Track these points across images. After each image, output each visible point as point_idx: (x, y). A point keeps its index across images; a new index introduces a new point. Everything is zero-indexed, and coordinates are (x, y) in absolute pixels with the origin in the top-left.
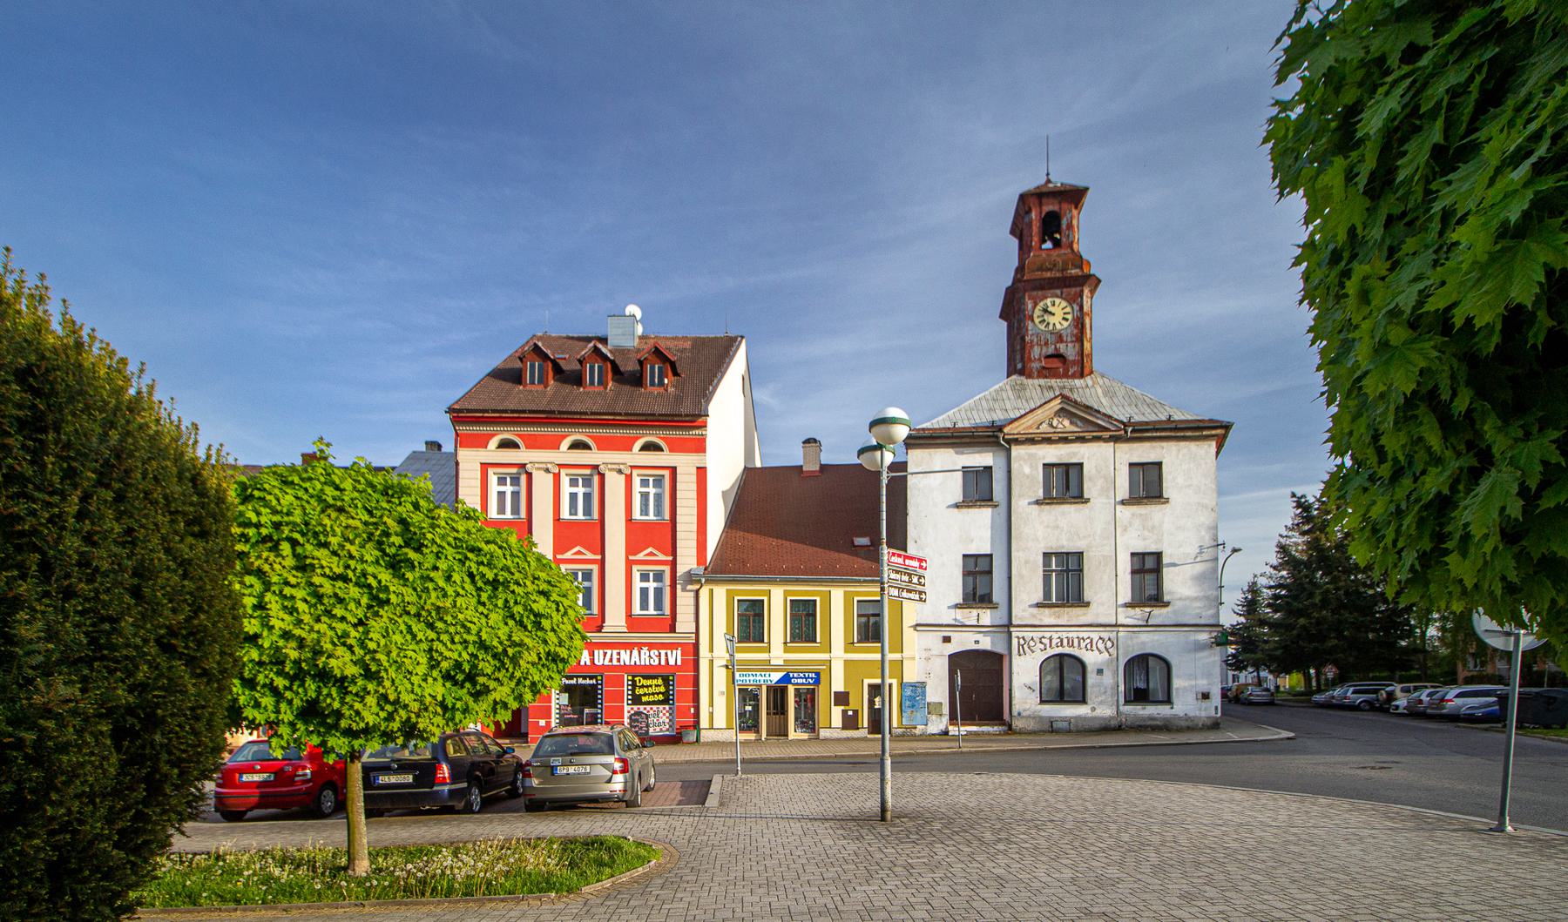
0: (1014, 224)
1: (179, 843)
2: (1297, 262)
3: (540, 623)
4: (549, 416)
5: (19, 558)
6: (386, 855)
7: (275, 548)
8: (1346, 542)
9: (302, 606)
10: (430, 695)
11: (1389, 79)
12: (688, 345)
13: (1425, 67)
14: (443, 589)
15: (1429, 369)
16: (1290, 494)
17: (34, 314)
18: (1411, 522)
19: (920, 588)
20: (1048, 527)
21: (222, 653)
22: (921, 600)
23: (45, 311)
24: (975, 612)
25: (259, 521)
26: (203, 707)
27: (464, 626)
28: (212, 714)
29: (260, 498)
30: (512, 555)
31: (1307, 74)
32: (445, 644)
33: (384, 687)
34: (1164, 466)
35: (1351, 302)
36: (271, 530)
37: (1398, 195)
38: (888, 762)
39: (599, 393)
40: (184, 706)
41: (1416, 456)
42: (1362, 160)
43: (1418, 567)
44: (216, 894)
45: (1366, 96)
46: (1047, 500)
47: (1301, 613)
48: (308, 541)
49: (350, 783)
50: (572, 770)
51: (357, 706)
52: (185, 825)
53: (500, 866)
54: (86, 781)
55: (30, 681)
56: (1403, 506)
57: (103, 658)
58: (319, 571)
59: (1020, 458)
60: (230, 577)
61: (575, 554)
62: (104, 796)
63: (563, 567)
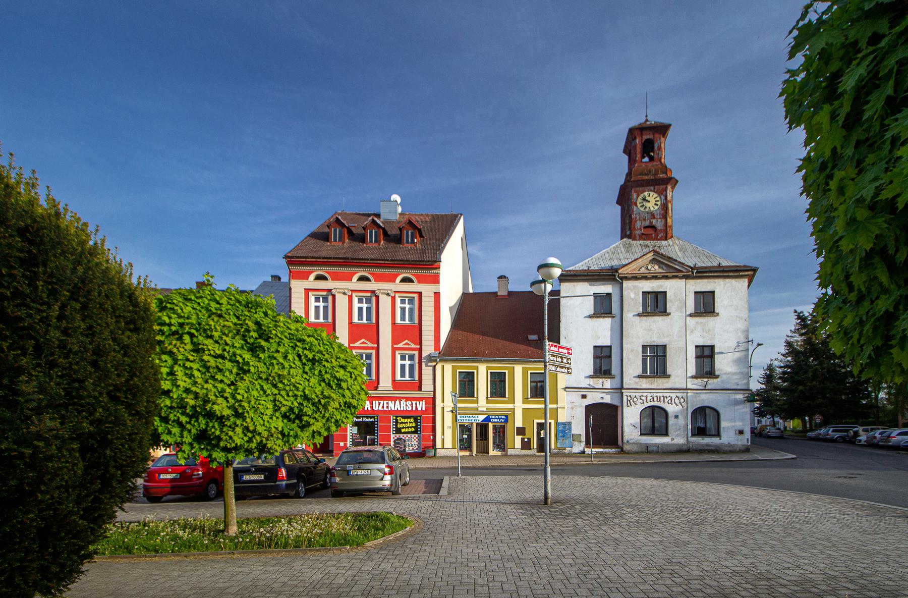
0: (626, 147)
1: (120, 516)
2: (799, 170)
3: (340, 385)
4: (346, 261)
5: (21, 343)
6: (248, 523)
7: (180, 339)
8: (828, 340)
9: (196, 373)
10: (274, 427)
11: (860, 55)
12: (429, 219)
13: (883, 48)
14: (282, 364)
15: (881, 235)
16: (793, 311)
17: (29, 194)
18: (869, 328)
19: (567, 366)
20: (645, 330)
21: (148, 401)
22: (568, 373)
23: (36, 193)
24: (601, 380)
25: (170, 322)
26: (136, 434)
27: (294, 386)
28: (142, 438)
29: (171, 308)
30: (324, 344)
31: (808, 53)
32: (283, 397)
33: (246, 422)
34: (716, 294)
35: (833, 194)
36: (178, 328)
37: (864, 128)
38: (549, 470)
39: (376, 248)
40: (124, 433)
41: (873, 288)
42: (841, 106)
43: (873, 355)
44: (143, 547)
45: (845, 66)
46: (645, 313)
47: (800, 383)
48: (200, 335)
49: (226, 480)
50: (359, 472)
51: (231, 433)
52: (125, 505)
53: (316, 530)
54: (63, 478)
55: (28, 418)
56: (864, 318)
57: (74, 404)
58: (207, 352)
59: (628, 288)
60: (153, 356)
61: (361, 343)
62: (74, 488)
63: (354, 352)
